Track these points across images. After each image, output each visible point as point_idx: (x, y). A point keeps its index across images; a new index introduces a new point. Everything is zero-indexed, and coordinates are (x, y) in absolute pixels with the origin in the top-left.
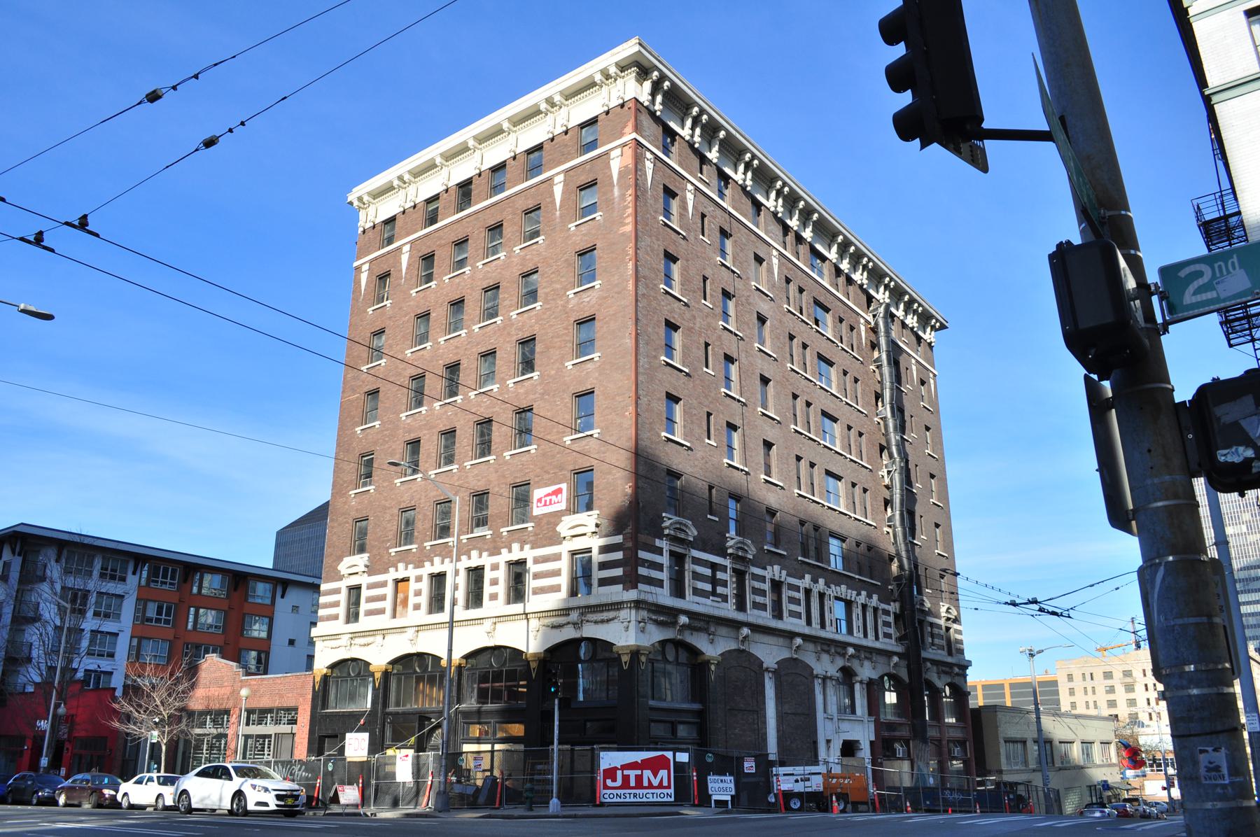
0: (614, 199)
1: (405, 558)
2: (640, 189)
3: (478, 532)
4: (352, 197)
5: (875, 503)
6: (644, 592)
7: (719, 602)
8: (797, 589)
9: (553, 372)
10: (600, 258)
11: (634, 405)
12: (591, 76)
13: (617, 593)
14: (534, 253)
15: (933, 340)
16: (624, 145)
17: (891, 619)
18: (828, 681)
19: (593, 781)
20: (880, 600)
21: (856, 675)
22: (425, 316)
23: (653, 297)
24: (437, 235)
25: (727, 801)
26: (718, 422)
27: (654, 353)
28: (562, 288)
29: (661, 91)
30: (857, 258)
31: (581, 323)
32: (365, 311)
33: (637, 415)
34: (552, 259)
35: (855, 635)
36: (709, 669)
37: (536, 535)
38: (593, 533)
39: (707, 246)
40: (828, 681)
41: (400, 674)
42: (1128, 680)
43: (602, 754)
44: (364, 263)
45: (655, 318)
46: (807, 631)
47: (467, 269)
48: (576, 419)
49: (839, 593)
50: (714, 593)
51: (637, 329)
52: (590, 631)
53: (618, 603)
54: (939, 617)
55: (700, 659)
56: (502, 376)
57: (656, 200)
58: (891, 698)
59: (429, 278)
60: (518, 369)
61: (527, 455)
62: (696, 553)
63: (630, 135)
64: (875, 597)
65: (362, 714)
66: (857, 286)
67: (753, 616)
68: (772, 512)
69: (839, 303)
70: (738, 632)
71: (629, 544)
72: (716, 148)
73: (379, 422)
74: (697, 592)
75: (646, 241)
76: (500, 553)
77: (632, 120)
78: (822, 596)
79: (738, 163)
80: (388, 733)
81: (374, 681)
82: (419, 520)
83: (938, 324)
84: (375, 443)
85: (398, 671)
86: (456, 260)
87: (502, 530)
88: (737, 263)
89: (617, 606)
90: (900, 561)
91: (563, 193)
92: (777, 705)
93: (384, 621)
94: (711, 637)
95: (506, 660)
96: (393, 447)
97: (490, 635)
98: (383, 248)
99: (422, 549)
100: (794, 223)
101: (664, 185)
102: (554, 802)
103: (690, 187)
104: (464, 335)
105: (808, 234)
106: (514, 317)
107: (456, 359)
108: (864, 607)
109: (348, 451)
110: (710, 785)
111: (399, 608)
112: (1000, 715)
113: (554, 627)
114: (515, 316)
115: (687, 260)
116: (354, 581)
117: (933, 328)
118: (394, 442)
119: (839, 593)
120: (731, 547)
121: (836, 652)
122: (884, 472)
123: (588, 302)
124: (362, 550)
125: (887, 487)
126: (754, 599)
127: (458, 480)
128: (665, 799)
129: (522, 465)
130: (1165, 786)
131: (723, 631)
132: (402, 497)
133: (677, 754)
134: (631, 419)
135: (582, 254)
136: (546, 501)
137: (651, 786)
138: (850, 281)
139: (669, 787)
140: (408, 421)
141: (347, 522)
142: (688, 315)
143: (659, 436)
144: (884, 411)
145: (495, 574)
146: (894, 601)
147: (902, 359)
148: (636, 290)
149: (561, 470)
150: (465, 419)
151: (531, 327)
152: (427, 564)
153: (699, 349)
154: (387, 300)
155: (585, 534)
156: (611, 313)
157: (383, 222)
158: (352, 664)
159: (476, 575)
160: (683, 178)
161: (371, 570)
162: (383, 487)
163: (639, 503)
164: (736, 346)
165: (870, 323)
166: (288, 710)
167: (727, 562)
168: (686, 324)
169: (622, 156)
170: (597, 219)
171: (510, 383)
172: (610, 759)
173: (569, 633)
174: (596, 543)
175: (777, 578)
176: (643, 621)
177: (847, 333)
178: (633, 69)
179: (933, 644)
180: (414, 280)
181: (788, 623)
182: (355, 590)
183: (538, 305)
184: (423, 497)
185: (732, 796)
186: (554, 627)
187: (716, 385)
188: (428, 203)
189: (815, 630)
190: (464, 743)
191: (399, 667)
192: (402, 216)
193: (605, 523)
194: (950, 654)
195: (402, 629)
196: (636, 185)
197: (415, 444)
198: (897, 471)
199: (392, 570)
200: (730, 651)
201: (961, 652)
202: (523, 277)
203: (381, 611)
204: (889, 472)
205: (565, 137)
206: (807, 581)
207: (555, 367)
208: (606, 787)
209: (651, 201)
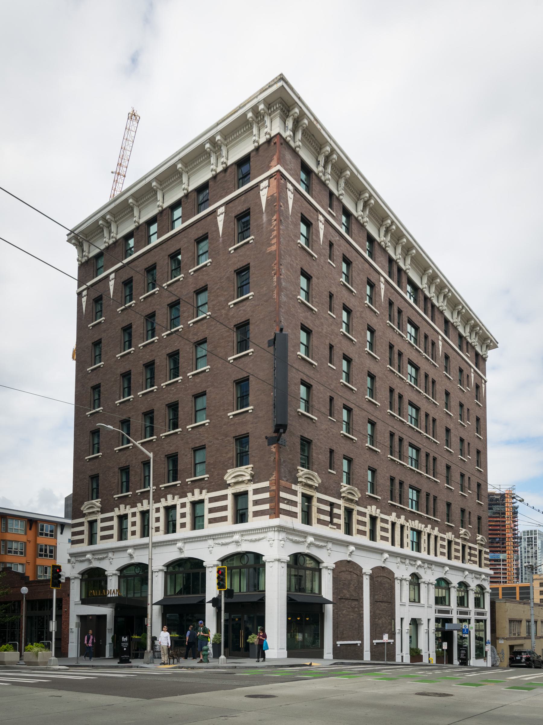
0: (263, 224)
1: (124, 500)
2: (283, 215)
6: (283, 520)
8: (386, 521)
16: (270, 177)
18: (404, 582)
20: (440, 531)
39: (333, 269)
49: (414, 525)
50: (331, 522)
56: (184, 370)
64: (436, 529)
67: (356, 538)
71: (274, 488)
74: (320, 521)
78: (402, 527)
93: (114, 543)
101: (302, 214)
103: (321, 218)
107: (151, 359)
108: (429, 535)
115: (318, 279)
119: (414, 525)
120: (344, 492)
129: (200, 434)
141: (85, 478)
145: (183, 510)
149: (226, 437)
151: (203, 332)
156: (261, 317)
159: (170, 510)
163: (280, 459)
167: (341, 502)
168: (316, 329)
169: (269, 186)
175: (374, 515)
176: (283, 540)
179: (470, 560)
181: (380, 544)
189: (397, 549)
200: (341, 561)
203: (111, 537)
206: (392, 517)
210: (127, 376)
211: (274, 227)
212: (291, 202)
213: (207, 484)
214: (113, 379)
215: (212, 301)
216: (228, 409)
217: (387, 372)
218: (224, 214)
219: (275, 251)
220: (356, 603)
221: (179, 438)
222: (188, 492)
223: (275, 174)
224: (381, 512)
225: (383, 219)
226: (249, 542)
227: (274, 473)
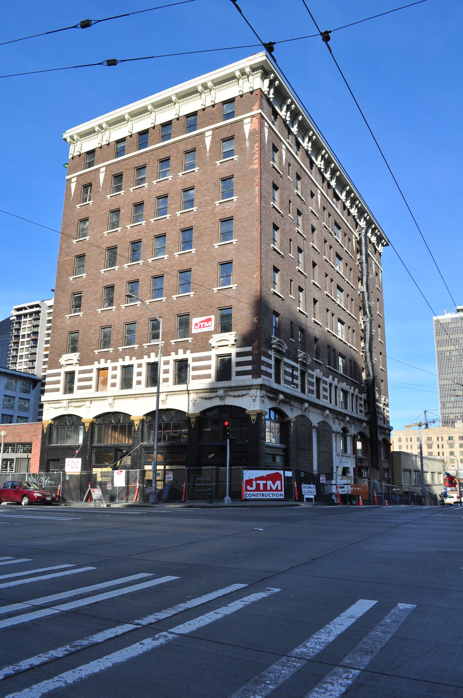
0: (246, 148)
1: (106, 356)
3: (154, 342)
4: (66, 135)
5: (357, 339)
7: (295, 388)
9: (205, 249)
10: (236, 183)
11: (259, 271)
12: (233, 72)
13: (249, 380)
14: (192, 177)
15: (382, 251)
16: (253, 116)
17: (362, 402)
19: (241, 486)
21: (348, 432)
22: (116, 212)
23: (268, 209)
24: (124, 162)
25: (313, 498)
26: (295, 285)
27: (268, 242)
28: (211, 200)
29: (273, 86)
30: (353, 200)
31: (223, 221)
32: (75, 207)
33: (261, 277)
34: (204, 181)
35: (348, 409)
36: (291, 425)
37: (194, 345)
38: (232, 345)
39: (291, 183)
40: (338, 435)
41: (101, 424)
42: (430, 442)
43: (244, 471)
44: (73, 177)
45: (269, 222)
46: (330, 406)
47: (146, 185)
48: (220, 278)
50: (292, 383)
51: (261, 227)
52: (230, 401)
53: (249, 386)
54: (380, 403)
55: (286, 419)
57: (269, 152)
58: (359, 445)
59: (119, 189)
60: (181, 247)
61: (188, 298)
62: (286, 360)
63: (257, 111)
65: (77, 447)
66: (352, 216)
68: (316, 340)
69: (345, 225)
70: (302, 405)
72: (296, 126)
73: (85, 274)
74: (286, 382)
75: (265, 175)
76: (171, 355)
77: (259, 101)
78: (336, 387)
79: (305, 136)
80: (94, 459)
81: (84, 428)
82: (114, 333)
83: (385, 243)
84: (83, 287)
85: (99, 422)
86: (137, 179)
87: (171, 341)
88: (303, 195)
89: (249, 387)
90: (368, 370)
91: (212, 142)
92: (317, 447)
94: (292, 407)
95: (173, 417)
96: (96, 289)
97: (111, 406)
98: (86, 169)
99: (116, 351)
100: (328, 176)
102: (227, 498)
103: (284, 147)
104: (144, 224)
105: (333, 183)
106: (178, 215)
107: (138, 238)
108: (353, 394)
109: (64, 291)
110: (303, 490)
111: (100, 386)
112: (402, 456)
113: (206, 398)
114: (179, 215)
115: (283, 190)
116: (69, 369)
117: (383, 245)
118: (96, 286)
120: (300, 357)
121: (341, 419)
122: (361, 322)
123: (229, 209)
124: (74, 350)
125: (362, 330)
126: (309, 387)
127: (141, 311)
128: (279, 497)
129: (185, 303)
130: (459, 496)
131: (296, 404)
132: (102, 320)
133: (286, 472)
134: (257, 279)
135: (224, 180)
136: (200, 325)
137: (271, 490)
138: (349, 213)
139: (281, 490)
140: (106, 274)
142: (282, 222)
143: (270, 291)
144: (362, 288)
145: (139, 370)
146: (364, 393)
147: (369, 259)
148: (261, 203)
149: (210, 308)
150: (145, 275)
151: (190, 221)
152: (120, 360)
153: (287, 243)
154: (90, 200)
155: (227, 345)
156: (244, 216)
157: (86, 152)
158: (68, 418)
159: (127, 369)
160: (281, 141)
161: (81, 362)
162: (89, 313)
164: (303, 243)
165: (357, 238)
166: (24, 444)
169: (251, 122)
170: (235, 159)
171: (176, 254)
172: (249, 474)
173: (216, 402)
174: (233, 351)
177: (348, 242)
178: (260, 71)
180: (109, 189)
181: (323, 402)
182: (70, 375)
183: (195, 209)
184: (117, 320)
185: (315, 496)
186: (206, 398)
187: (294, 264)
188: (117, 143)
190: (145, 465)
191: (99, 420)
192: (100, 150)
193: (239, 338)
194: (384, 423)
195: (104, 398)
196: (261, 141)
197: (111, 288)
198: (369, 322)
199: (96, 363)
200: (299, 416)
201: (388, 422)
202: (184, 191)
204: (364, 322)
205: (213, 109)
206: (329, 380)
207: (206, 246)
208: (247, 490)
209: (267, 152)
210: (112, 250)
211: (256, 151)
212: (266, 135)
213: (191, 345)
214: (99, 251)
215: (199, 199)
216: (212, 285)
217: (323, 261)
218: (211, 136)
219: (257, 169)
220: (308, 452)
221: (164, 305)
222: (172, 352)
223: (257, 115)
224: (323, 375)
225: (320, 149)
226: (232, 397)
227: (257, 340)
